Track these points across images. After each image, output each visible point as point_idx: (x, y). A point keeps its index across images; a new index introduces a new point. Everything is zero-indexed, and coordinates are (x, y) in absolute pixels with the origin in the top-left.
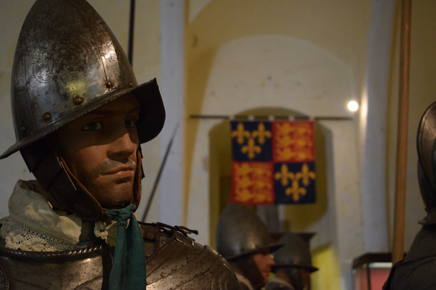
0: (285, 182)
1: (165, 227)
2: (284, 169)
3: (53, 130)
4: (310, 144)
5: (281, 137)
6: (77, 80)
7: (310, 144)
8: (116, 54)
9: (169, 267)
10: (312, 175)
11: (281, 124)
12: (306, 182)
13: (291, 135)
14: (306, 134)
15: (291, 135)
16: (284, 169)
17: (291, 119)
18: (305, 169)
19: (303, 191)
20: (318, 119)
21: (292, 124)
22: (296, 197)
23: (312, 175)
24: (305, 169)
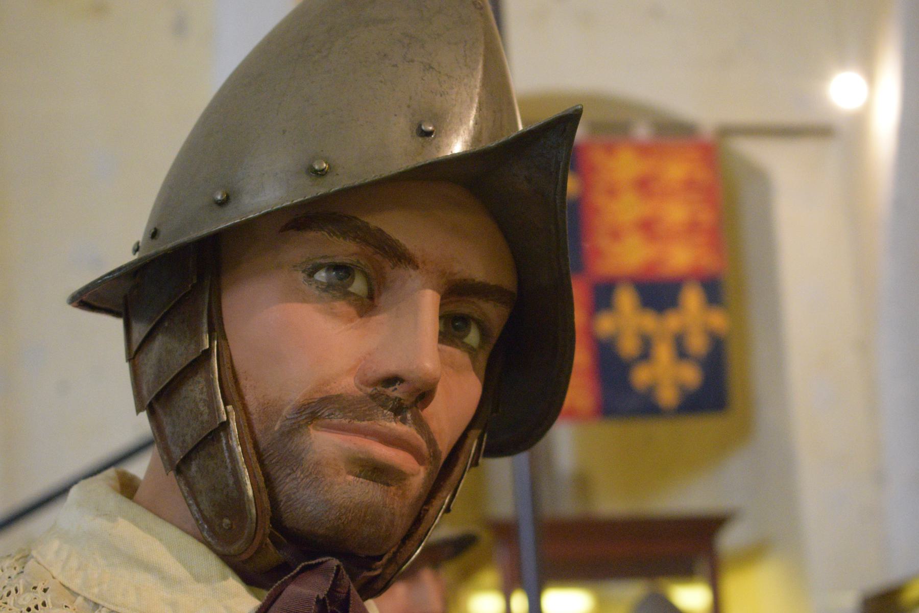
0: (629, 346)
1: (485, 66)
2: (626, 299)
3: (243, 219)
4: (705, 216)
5: (612, 192)
6: (641, 347)
7: (705, 216)
8: (496, 332)
9: (301, 430)
10: (718, 320)
11: (610, 149)
12: (698, 344)
13: (644, 185)
14: (690, 185)
15: (644, 185)
16: (626, 299)
17: (642, 132)
18: (692, 299)
19: (691, 375)
20: (728, 132)
21: (644, 150)
22: (668, 396)
23: (718, 320)
24: (692, 299)
